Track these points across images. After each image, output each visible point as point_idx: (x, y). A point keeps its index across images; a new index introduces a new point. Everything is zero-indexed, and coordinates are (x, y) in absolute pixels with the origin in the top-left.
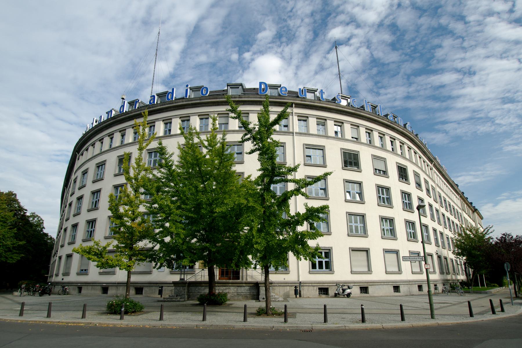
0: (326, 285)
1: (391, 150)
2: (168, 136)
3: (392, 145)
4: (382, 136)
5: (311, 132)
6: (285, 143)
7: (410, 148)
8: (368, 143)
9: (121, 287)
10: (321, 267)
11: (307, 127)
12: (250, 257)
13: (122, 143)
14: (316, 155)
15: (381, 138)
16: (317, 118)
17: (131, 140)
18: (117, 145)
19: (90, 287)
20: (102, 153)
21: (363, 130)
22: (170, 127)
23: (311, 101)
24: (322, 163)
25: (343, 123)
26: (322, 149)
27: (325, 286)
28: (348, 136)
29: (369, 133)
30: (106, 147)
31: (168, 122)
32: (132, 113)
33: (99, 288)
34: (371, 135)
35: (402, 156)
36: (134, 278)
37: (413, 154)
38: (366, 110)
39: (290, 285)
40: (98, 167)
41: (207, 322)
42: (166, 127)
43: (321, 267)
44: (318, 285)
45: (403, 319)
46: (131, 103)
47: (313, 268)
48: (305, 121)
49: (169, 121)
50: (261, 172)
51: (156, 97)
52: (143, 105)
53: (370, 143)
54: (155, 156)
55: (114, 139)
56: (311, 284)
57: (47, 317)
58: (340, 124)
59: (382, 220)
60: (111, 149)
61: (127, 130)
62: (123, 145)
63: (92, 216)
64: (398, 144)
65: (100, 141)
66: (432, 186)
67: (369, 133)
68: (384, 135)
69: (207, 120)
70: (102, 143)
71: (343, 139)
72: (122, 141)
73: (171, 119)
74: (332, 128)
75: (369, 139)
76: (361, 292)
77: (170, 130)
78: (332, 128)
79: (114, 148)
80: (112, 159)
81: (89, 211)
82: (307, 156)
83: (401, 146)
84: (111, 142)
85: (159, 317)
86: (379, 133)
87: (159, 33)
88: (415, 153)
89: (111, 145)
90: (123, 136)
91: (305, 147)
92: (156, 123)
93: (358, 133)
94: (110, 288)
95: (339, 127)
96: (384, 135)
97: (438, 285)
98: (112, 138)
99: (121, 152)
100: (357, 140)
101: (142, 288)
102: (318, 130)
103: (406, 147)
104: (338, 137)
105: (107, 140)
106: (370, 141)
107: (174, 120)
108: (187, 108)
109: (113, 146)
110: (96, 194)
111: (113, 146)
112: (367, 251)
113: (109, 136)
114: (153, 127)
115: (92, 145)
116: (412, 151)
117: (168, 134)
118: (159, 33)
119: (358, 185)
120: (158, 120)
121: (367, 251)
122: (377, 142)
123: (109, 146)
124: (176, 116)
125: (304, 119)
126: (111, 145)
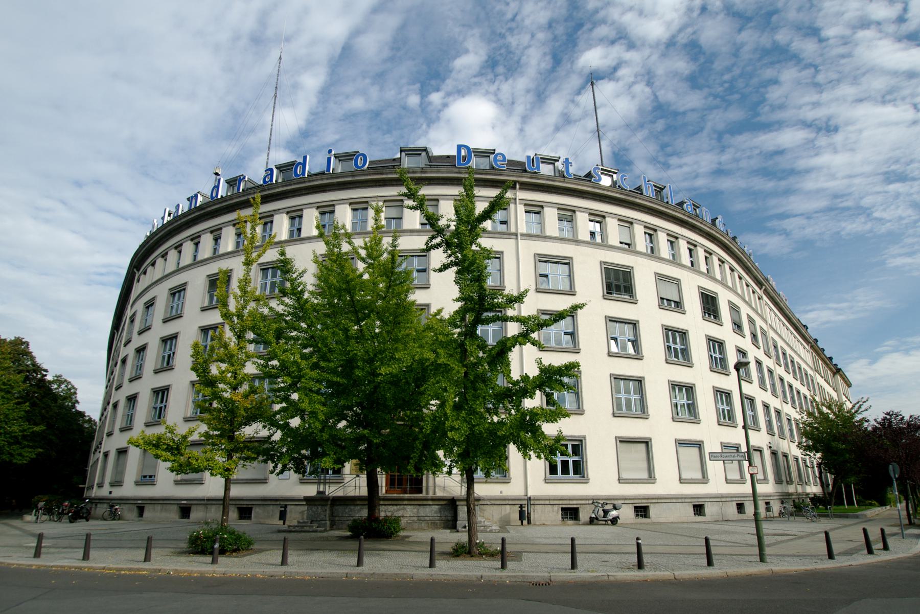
0: (575, 502)
1: (689, 265)
2: (297, 240)
3: (691, 256)
4: (673, 240)
5: (548, 233)
6: (502, 252)
7: (722, 261)
8: (649, 252)
9: (214, 507)
10: (565, 471)
11: (541, 223)
12: (440, 453)
13: (214, 253)
14: (558, 273)
15: (672, 243)
16: (559, 209)
17: (230, 247)
18: (206, 256)
19: (159, 507)
20: (179, 270)
21: (639, 230)
22: (300, 223)
23: (548, 178)
24: (568, 288)
25: (604, 217)
26: (567, 262)
27: (573, 504)
28: (614, 240)
29: (650, 235)
30: (187, 259)
31: (296, 216)
32: (232, 199)
33: (175, 508)
34: (654, 238)
35: (709, 274)
36: (236, 491)
37: (728, 271)
38: (645, 193)
39: (510, 502)
40: (173, 294)
41: (366, 568)
42: (292, 225)
43: (565, 471)
44: (561, 502)
45: (710, 563)
46: (232, 183)
47: (551, 473)
48: (538, 213)
49: (298, 213)
50: (459, 304)
51: (275, 171)
52: (252, 185)
53: (652, 252)
54: (274, 276)
55: (201, 245)
56: (548, 501)
57: (84, 559)
58: (599, 219)
59: (674, 389)
60: (196, 263)
61: (224, 229)
62: (216, 256)
63: (162, 380)
64: (701, 254)
65: (176, 248)
66: (761, 327)
67: (650, 235)
68: (677, 238)
69: (365, 212)
70: (180, 252)
71: (605, 245)
72: (215, 249)
73: (302, 210)
74: (584, 226)
75: (650, 245)
76: (637, 516)
77: (299, 230)
78: (584, 226)
79: (201, 261)
80: (197, 281)
81: (157, 372)
82: (541, 275)
83: (706, 258)
84: (196, 250)
85: (280, 560)
86: (668, 235)
87: (280, 58)
88: (732, 270)
89: (195, 256)
90: (217, 240)
91: (538, 259)
92: (275, 217)
93: (632, 235)
94: (193, 508)
95: (598, 225)
96: (677, 238)
97: (772, 503)
98: (197, 244)
99: (214, 268)
100: (628, 246)
101: (251, 509)
102: (561, 230)
103: (715, 259)
104: (596, 241)
105: (188, 247)
106: (652, 248)
107: (306, 213)
108: (330, 191)
109: (199, 258)
110: (169, 343)
111: (199, 258)
112: (647, 443)
113: (192, 240)
114: (269, 225)
115: (163, 257)
116: (727, 267)
117: (296, 236)
118: (280, 58)
119: (631, 326)
120: (278, 211)
121: (647, 443)
122: (664, 250)
123: (192, 258)
124: (310, 205)
125: (535, 209)
126: (195, 256)
